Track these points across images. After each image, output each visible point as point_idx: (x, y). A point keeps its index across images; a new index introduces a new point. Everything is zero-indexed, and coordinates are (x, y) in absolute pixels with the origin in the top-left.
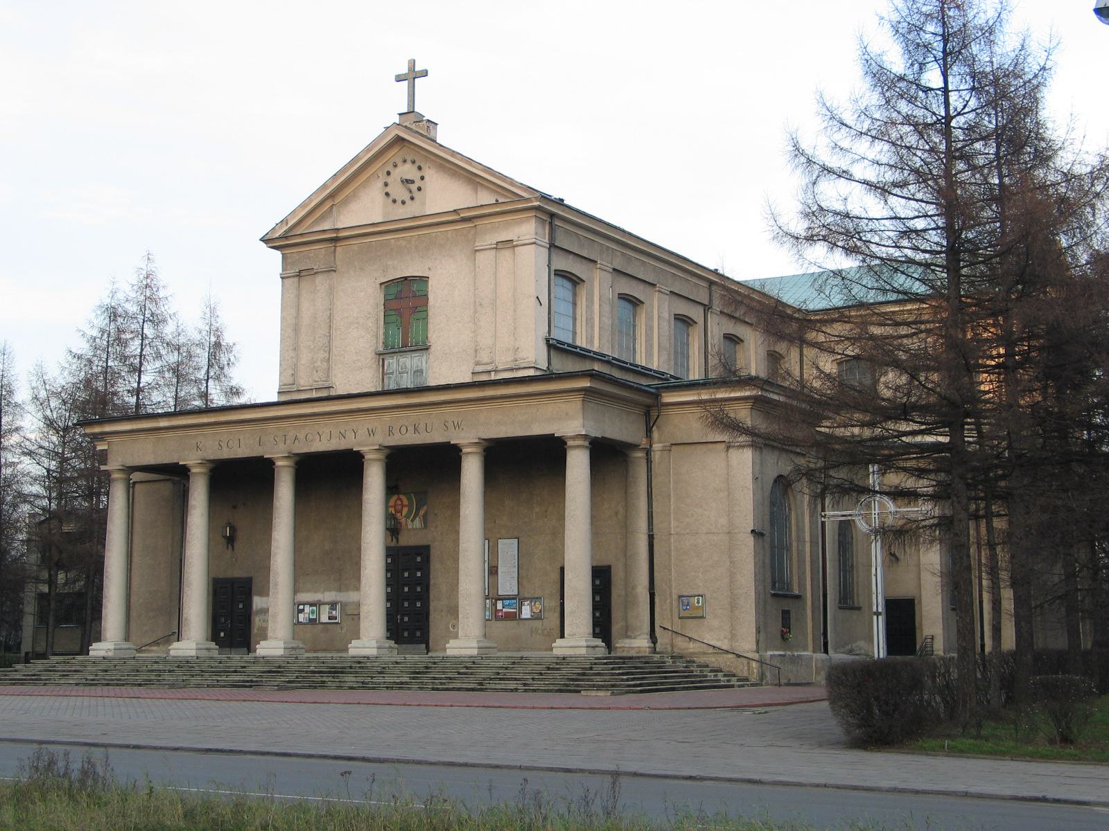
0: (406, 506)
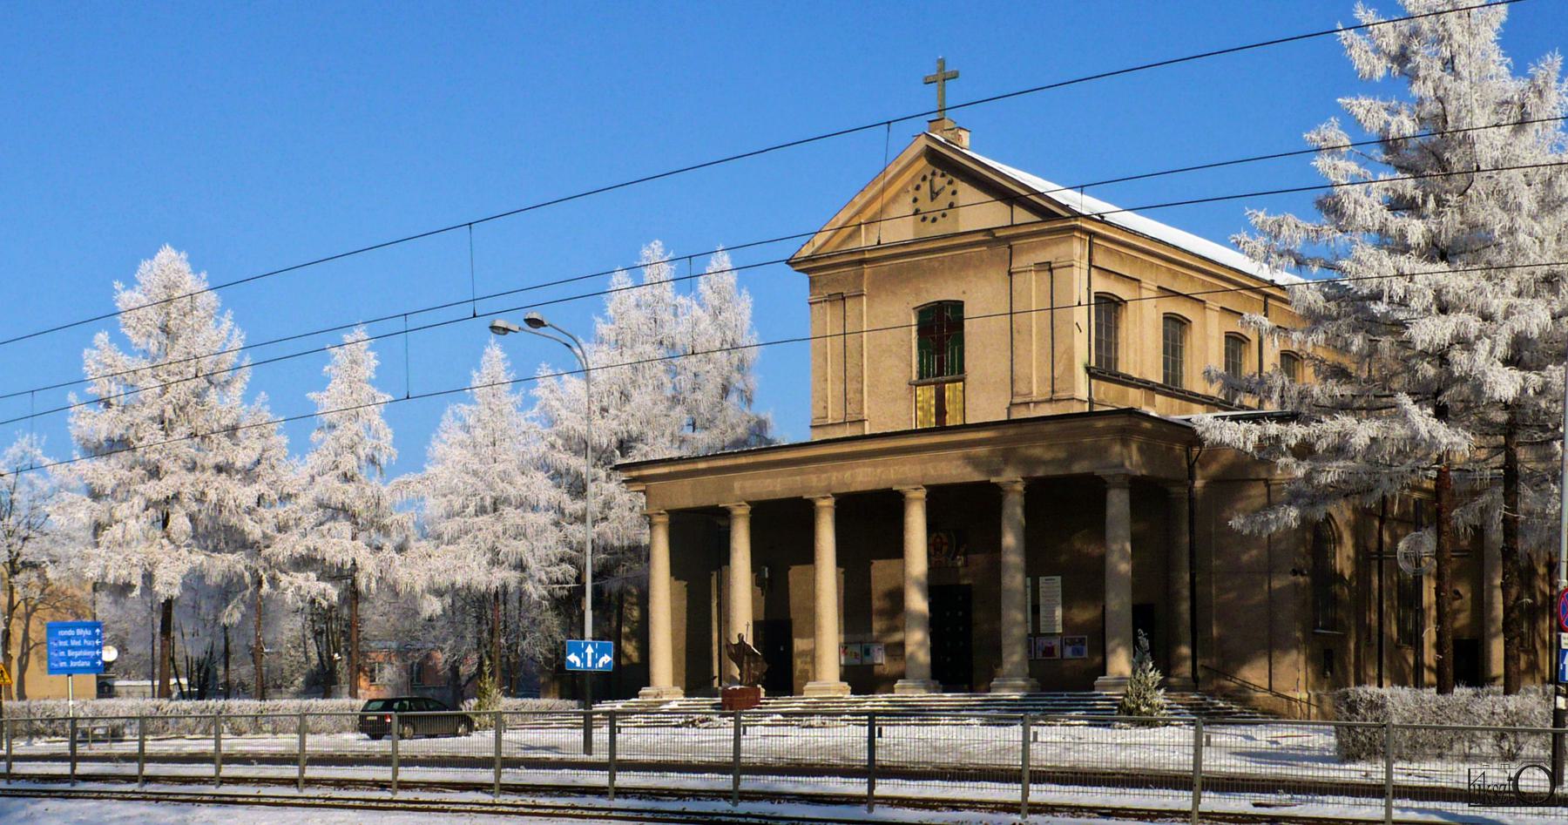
0: (946, 544)
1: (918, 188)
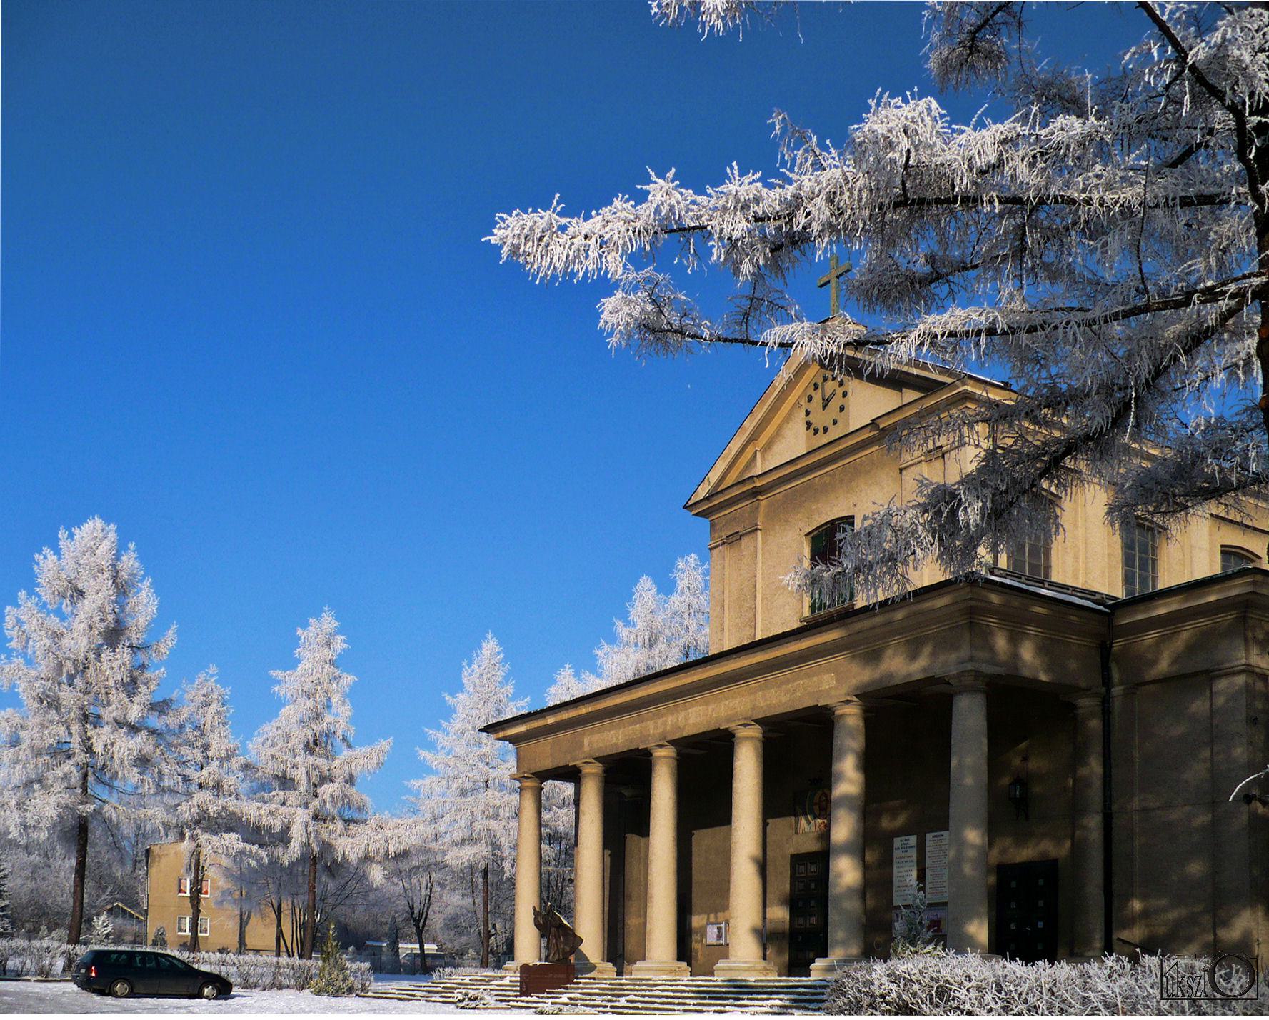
1: (810, 399)
